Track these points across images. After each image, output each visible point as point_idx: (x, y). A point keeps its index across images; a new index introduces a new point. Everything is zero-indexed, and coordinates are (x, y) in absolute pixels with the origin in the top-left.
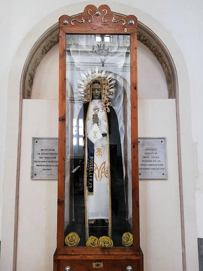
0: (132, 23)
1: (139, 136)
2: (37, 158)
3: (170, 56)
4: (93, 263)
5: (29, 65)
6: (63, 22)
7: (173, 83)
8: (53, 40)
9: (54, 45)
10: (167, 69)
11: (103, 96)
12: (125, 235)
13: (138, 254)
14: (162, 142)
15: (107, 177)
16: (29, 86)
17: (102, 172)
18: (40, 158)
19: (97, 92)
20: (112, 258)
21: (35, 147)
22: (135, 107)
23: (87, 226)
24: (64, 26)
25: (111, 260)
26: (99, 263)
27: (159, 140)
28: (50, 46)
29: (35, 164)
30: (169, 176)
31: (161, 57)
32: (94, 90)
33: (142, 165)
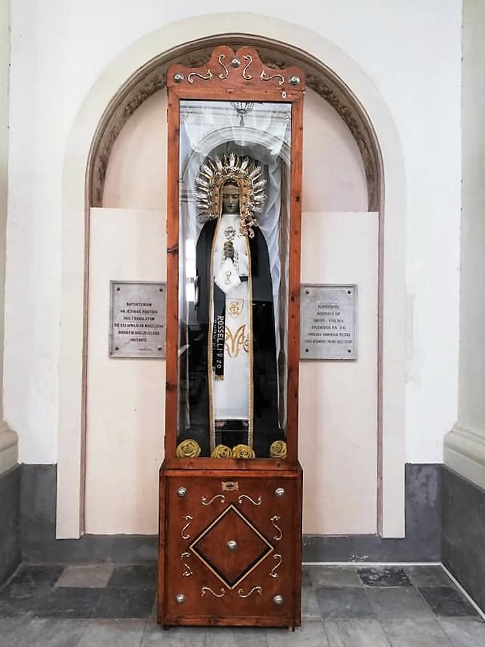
0: (296, 82)
1: (304, 280)
2: (120, 318)
3: (371, 127)
4: (223, 483)
5: (99, 141)
6: (174, 77)
7: (375, 182)
8: (146, 88)
9: (145, 98)
10: (367, 152)
11: (242, 208)
12: (275, 444)
13: (295, 468)
14: (118, 289)
15: (247, 351)
16: (99, 181)
17: (238, 343)
18: (125, 318)
19: (231, 200)
20: (253, 474)
21: (116, 298)
22: (296, 233)
23: (213, 430)
24: (176, 84)
25: (252, 478)
26: (232, 483)
27: (345, 289)
28: (138, 100)
29: (116, 329)
30: (359, 354)
31: (356, 127)
32: (226, 196)
33: (311, 334)
